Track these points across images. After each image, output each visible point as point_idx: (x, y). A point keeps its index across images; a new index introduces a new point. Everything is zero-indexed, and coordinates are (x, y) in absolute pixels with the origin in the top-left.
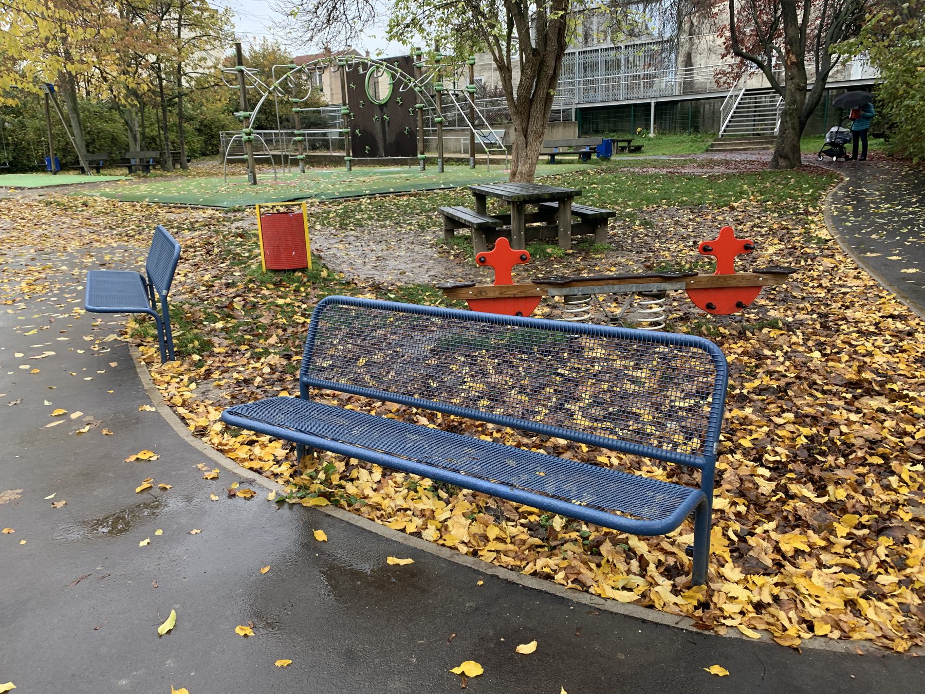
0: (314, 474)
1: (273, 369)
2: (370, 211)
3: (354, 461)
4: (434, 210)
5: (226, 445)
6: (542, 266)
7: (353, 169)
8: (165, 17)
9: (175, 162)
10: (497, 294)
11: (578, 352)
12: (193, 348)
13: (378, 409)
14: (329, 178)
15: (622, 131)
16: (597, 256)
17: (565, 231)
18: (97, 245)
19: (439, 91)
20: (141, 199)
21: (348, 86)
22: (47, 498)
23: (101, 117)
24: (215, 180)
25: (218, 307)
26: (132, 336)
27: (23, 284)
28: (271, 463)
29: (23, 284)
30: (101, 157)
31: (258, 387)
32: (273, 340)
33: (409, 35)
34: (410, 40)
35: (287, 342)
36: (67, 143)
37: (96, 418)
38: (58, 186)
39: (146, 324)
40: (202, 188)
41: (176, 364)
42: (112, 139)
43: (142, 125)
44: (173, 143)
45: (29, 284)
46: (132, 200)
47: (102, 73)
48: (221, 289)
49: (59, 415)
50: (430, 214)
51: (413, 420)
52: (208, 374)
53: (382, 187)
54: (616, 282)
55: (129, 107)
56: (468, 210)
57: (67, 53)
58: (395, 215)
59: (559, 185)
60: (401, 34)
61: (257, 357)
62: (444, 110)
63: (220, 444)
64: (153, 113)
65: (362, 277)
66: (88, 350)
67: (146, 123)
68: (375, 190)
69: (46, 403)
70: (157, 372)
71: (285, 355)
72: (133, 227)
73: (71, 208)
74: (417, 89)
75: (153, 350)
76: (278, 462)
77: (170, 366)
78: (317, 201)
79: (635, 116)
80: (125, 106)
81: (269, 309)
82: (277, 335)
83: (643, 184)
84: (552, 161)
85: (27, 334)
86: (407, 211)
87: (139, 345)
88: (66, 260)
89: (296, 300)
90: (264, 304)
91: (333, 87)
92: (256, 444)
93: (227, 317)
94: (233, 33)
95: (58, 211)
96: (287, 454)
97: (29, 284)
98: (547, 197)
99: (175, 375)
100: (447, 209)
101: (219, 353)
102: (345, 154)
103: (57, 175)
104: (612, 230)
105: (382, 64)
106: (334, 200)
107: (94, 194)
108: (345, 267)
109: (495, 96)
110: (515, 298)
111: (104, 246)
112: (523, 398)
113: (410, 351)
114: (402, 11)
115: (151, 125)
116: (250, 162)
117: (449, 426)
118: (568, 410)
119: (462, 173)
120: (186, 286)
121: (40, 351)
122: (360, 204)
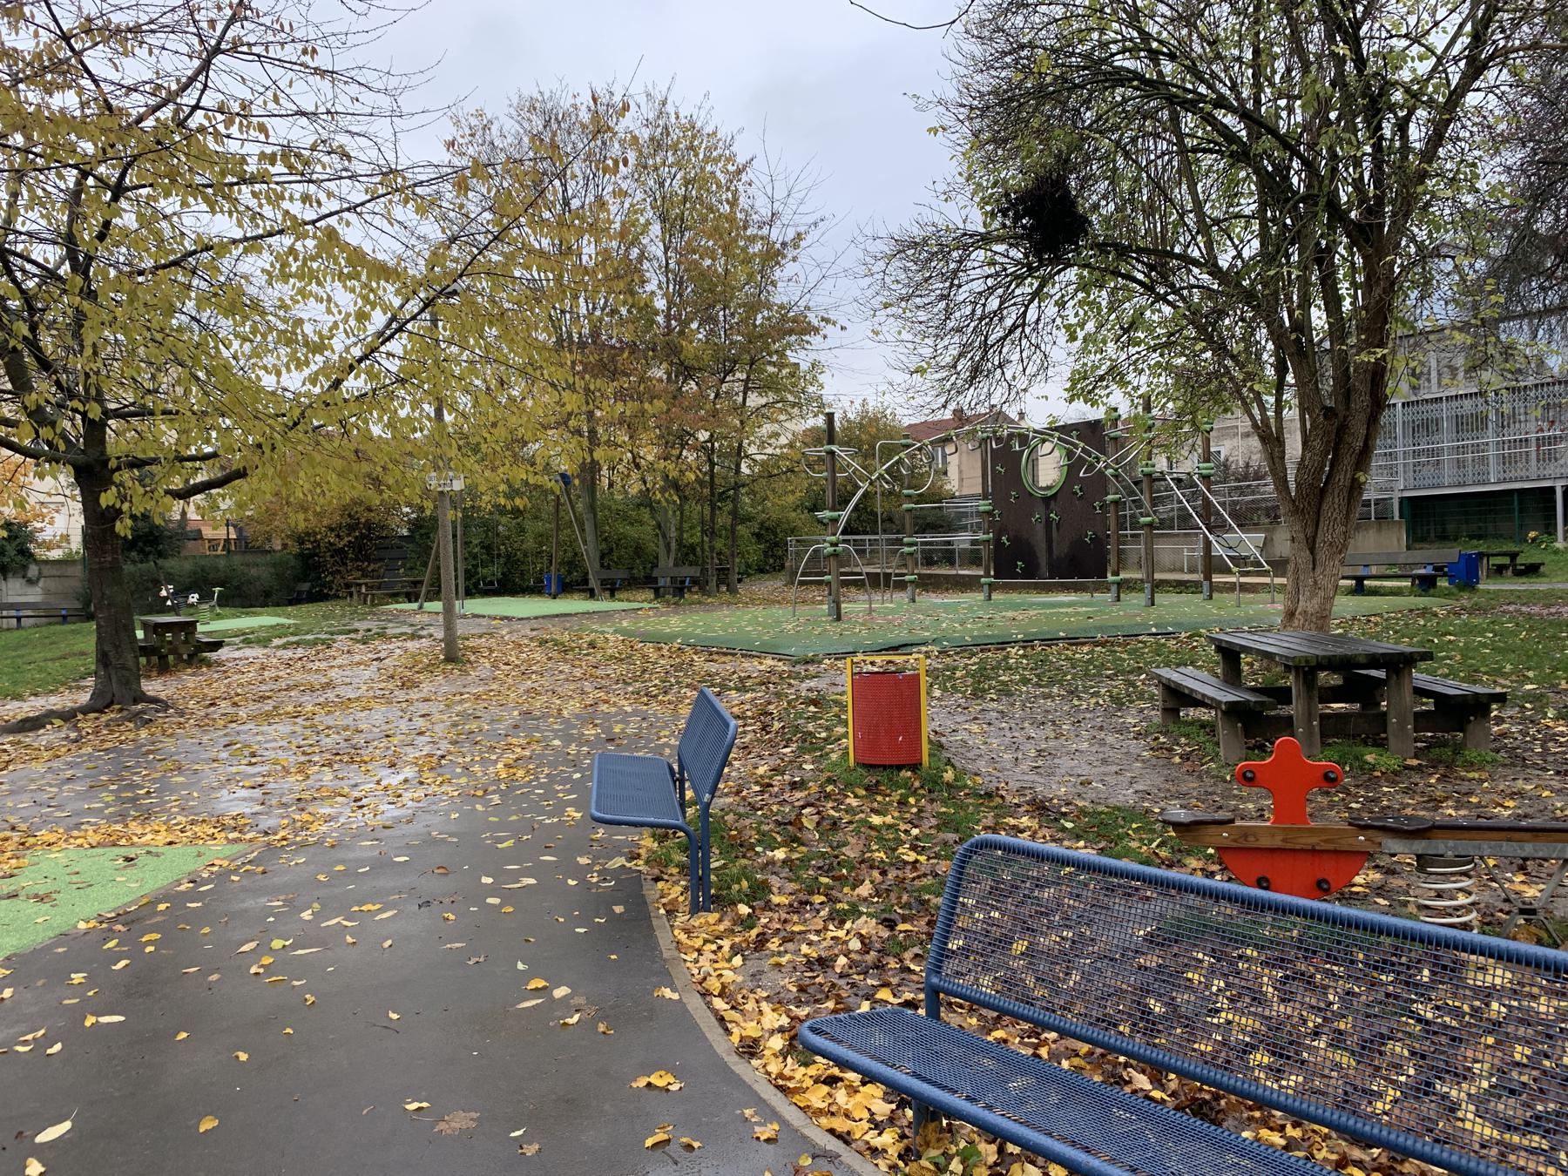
0: (942, 1160)
1: (866, 946)
2: (1024, 669)
3: (1011, 1148)
4: (1139, 670)
5: (791, 1078)
6: (1357, 786)
7: (994, 596)
8: (728, 379)
9: (720, 582)
10: (1277, 842)
11: (1453, 970)
12: (739, 891)
13: (1053, 1046)
14: (956, 611)
15: (1498, 536)
16: (1471, 775)
17: (1402, 724)
18: (604, 707)
19: (1149, 475)
20: (671, 638)
21: (993, 470)
22: (513, 1135)
23: (625, 518)
24: (777, 612)
25: (778, 823)
26: (647, 862)
27: (500, 765)
28: (865, 1125)
29: (500, 765)
30: (619, 574)
31: (841, 976)
32: (865, 890)
33: (1103, 393)
34: (1104, 399)
35: (888, 896)
36: (576, 554)
37: (590, 1002)
38: (557, 616)
39: (667, 844)
40: (759, 624)
41: (713, 917)
42: (636, 548)
43: (680, 529)
44: (719, 554)
45: (508, 766)
46: (658, 640)
47: (634, 458)
48: (782, 791)
49: (537, 989)
50: (1132, 678)
51: (1121, 1077)
52: (762, 941)
53: (1046, 629)
54: (1528, 835)
55: (664, 504)
56: (1204, 675)
57: (592, 432)
58: (1069, 677)
59: (1377, 636)
60: (1090, 392)
61: (839, 918)
62: (1155, 502)
63: (781, 1076)
64: (695, 510)
65: (1014, 785)
66: (583, 881)
67: (685, 525)
68: (1033, 634)
69: (520, 966)
70: (683, 930)
71: (886, 920)
72: (657, 682)
73: (572, 649)
74: (1109, 472)
75: (678, 889)
76: (878, 1127)
77: (702, 920)
78: (935, 649)
79: (1521, 510)
80: (659, 502)
81: (858, 832)
82: (872, 882)
83: (1554, 637)
84: (1359, 589)
86: (1093, 671)
87: (657, 879)
88: (559, 730)
89: (902, 819)
90: (850, 822)
91: (963, 468)
92: (839, 1084)
93: (793, 841)
94: (820, 397)
95: (554, 654)
96: (892, 1111)
97: (508, 766)
98: (1362, 660)
99: (711, 938)
100: (1167, 673)
101: (778, 905)
102: (982, 573)
104: (1497, 724)
105: (1052, 436)
106: (964, 649)
108: (982, 765)
109: (1246, 477)
110: (1314, 851)
111: (613, 710)
112: (1345, 1060)
113: (1111, 933)
114: (1092, 357)
115: (691, 528)
116: (834, 586)
117: (1194, 1099)
118: (1445, 1097)
119: (1189, 607)
120: (731, 783)
122: (1007, 657)
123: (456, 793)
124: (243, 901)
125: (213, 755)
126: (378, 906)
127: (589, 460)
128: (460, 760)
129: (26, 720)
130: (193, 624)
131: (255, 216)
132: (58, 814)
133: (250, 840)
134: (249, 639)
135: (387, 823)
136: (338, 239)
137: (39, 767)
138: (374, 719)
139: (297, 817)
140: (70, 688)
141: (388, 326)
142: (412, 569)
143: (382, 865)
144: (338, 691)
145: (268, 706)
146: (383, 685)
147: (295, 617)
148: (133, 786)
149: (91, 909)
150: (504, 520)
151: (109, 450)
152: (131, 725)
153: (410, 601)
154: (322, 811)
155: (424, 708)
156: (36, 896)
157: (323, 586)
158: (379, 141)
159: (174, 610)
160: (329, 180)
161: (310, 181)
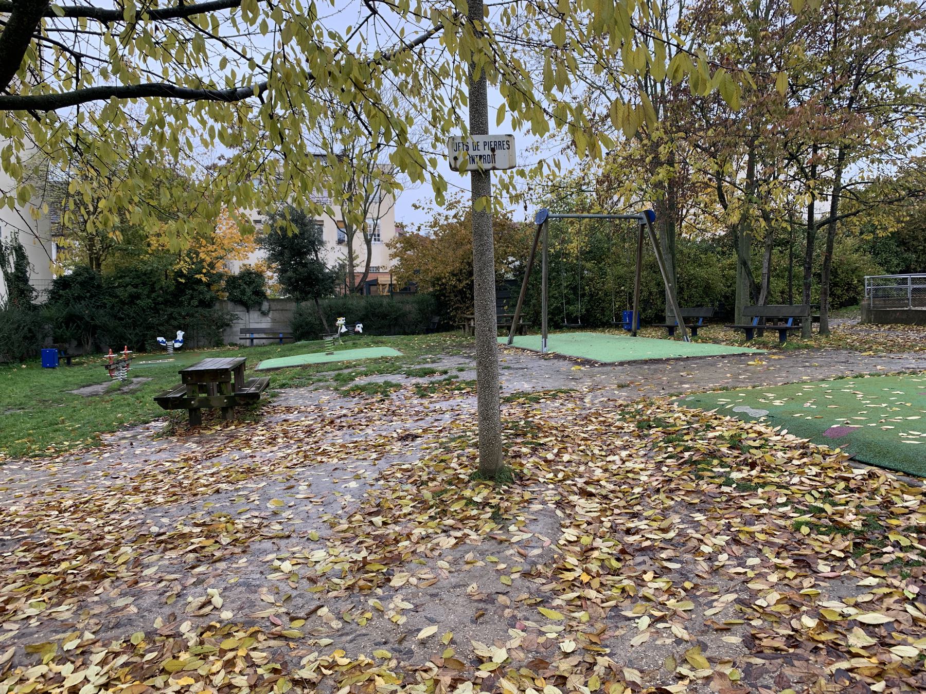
38: (645, 362)
103: (638, 338)
127: (473, 483)
157: (450, 319)
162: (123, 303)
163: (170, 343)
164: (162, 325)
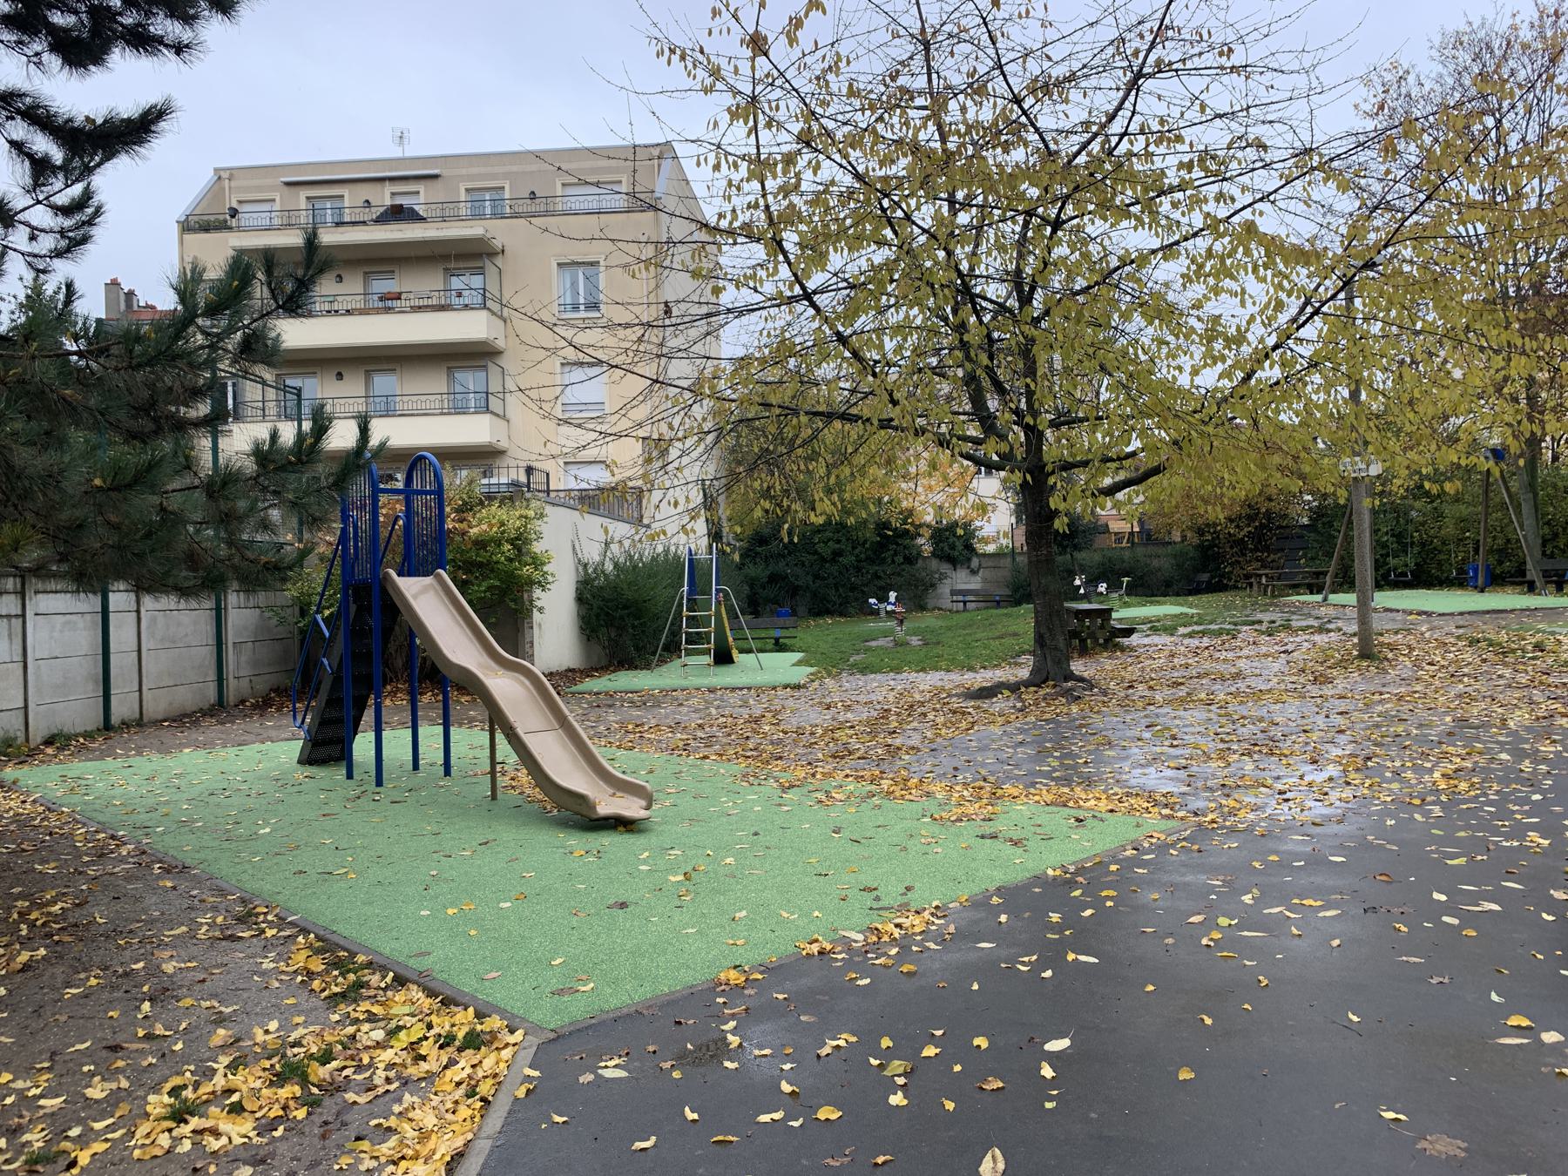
27: (1437, 775)
29: (1437, 775)
36: (1508, 541)
38: (1488, 612)
49: (1519, 1027)
73: (1513, 651)
85: (1449, 862)
95: (1490, 656)
107: (1557, 630)
121: (1475, 899)
123: (1389, 799)
124: (1183, 875)
125: (1138, 734)
126: (1319, 903)
128: (1389, 764)
129: (982, 689)
130: (1110, 611)
131: (1174, 224)
132: (1016, 772)
133: (1182, 819)
134: (1156, 627)
135: (1318, 820)
136: (1256, 231)
137: (996, 730)
138: (1288, 712)
139: (1224, 802)
140: (1010, 664)
141: (1302, 310)
142: (1312, 559)
143: (1316, 861)
144: (1249, 681)
145: (1182, 692)
146: (1294, 679)
147: (1196, 607)
148: (1071, 755)
149: (1056, 859)
150: (1418, 504)
151: (1046, 458)
152: (1064, 700)
153: (1312, 593)
154: (1247, 800)
155: (1342, 705)
156: (1011, 840)
158: (1295, 123)
159: (1086, 597)
160: (1241, 174)
161: (1224, 179)
162: (824, 560)
163: (882, 606)
164: (863, 585)
